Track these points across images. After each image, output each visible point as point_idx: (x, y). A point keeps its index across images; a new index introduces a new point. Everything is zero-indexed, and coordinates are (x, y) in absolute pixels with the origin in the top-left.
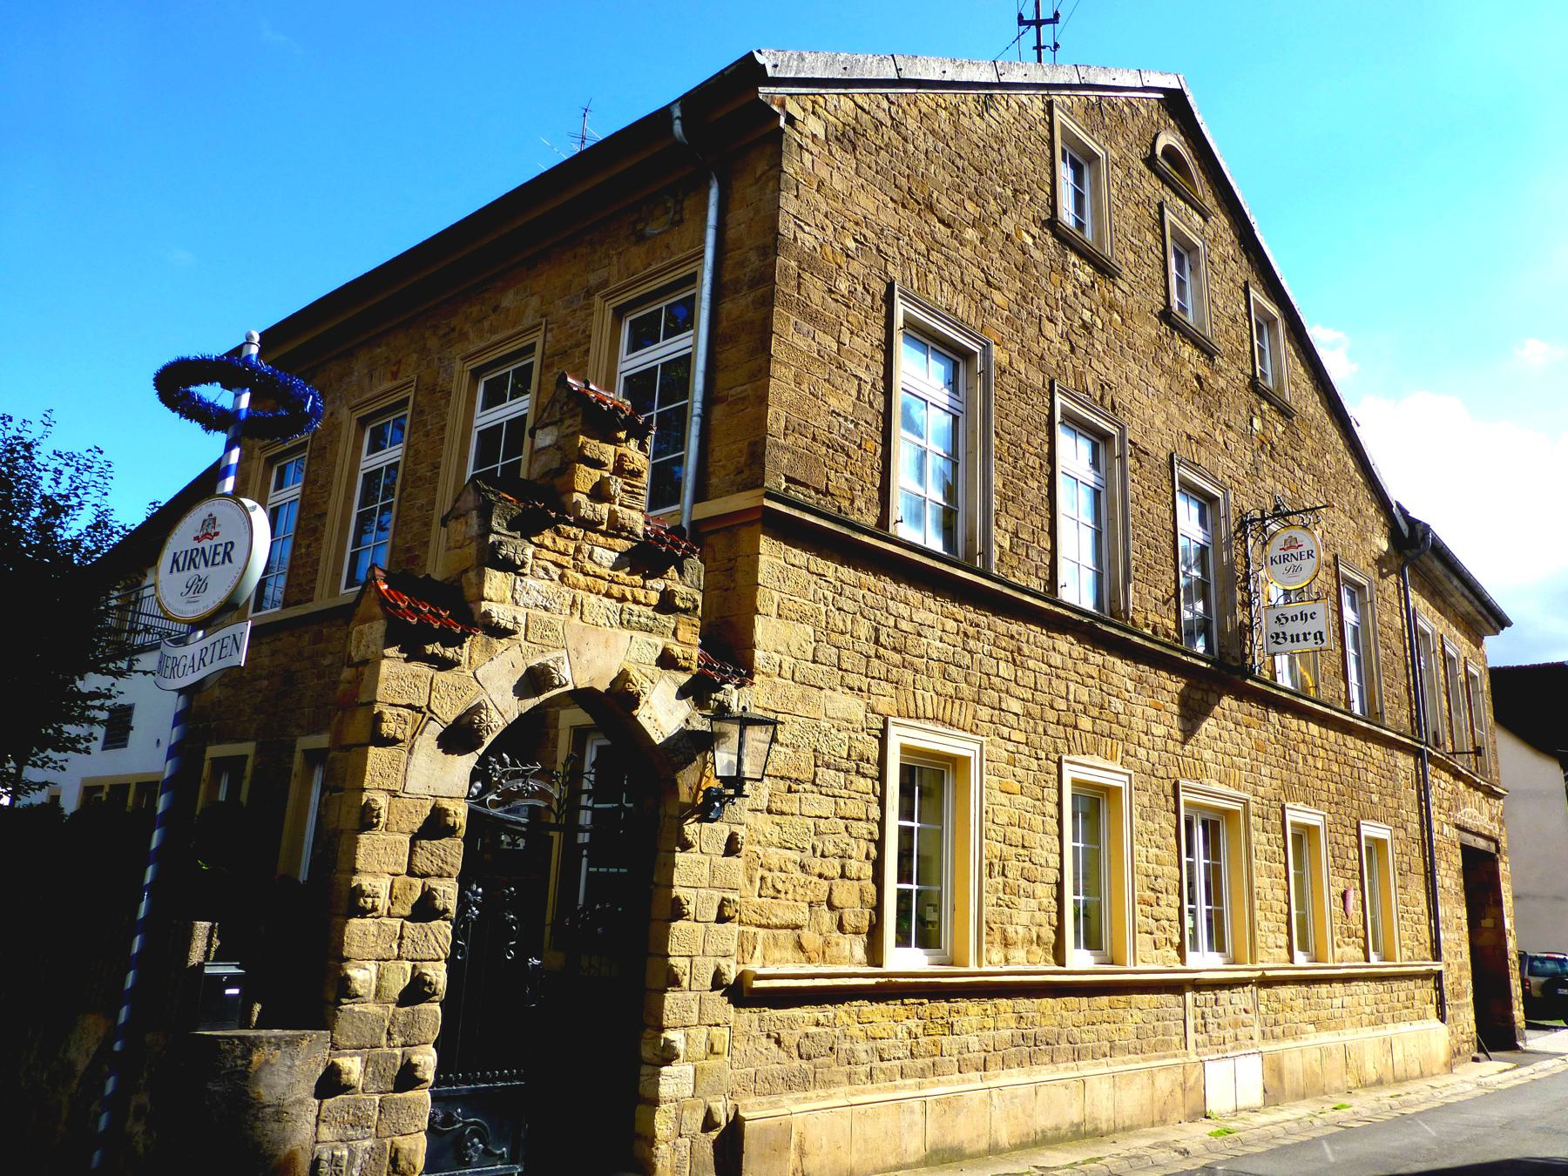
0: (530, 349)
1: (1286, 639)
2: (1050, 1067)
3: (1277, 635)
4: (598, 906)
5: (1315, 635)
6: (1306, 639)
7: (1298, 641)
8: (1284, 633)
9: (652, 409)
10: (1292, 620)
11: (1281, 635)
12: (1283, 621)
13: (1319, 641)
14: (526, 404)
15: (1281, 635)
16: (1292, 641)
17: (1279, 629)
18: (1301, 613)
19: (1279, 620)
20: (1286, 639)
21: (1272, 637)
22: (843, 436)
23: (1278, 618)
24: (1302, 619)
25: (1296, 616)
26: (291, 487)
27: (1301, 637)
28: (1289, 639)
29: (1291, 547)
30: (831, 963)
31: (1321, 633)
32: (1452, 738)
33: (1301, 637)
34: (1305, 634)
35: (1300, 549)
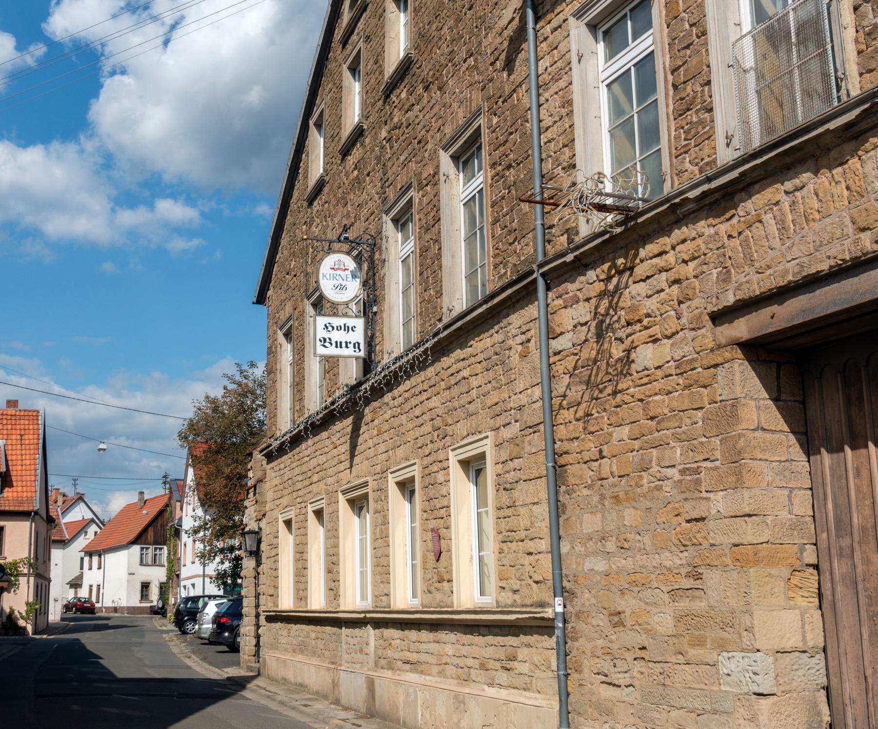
1: (331, 344)
2: (387, 491)
4: (227, 634)
5: (354, 344)
6: (347, 347)
7: (341, 347)
8: (330, 339)
10: (337, 329)
11: (328, 340)
12: (330, 328)
13: (357, 350)
15: (328, 340)
16: (337, 347)
18: (345, 325)
19: (327, 328)
20: (331, 344)
24: (345, 330)
25: (341, 327)
27: (344, 345)
28: (334, 344)
30: (501, 551)
31: (359, 344)
32: (832, 41)
33: (344, 345)
34: (346, 343)
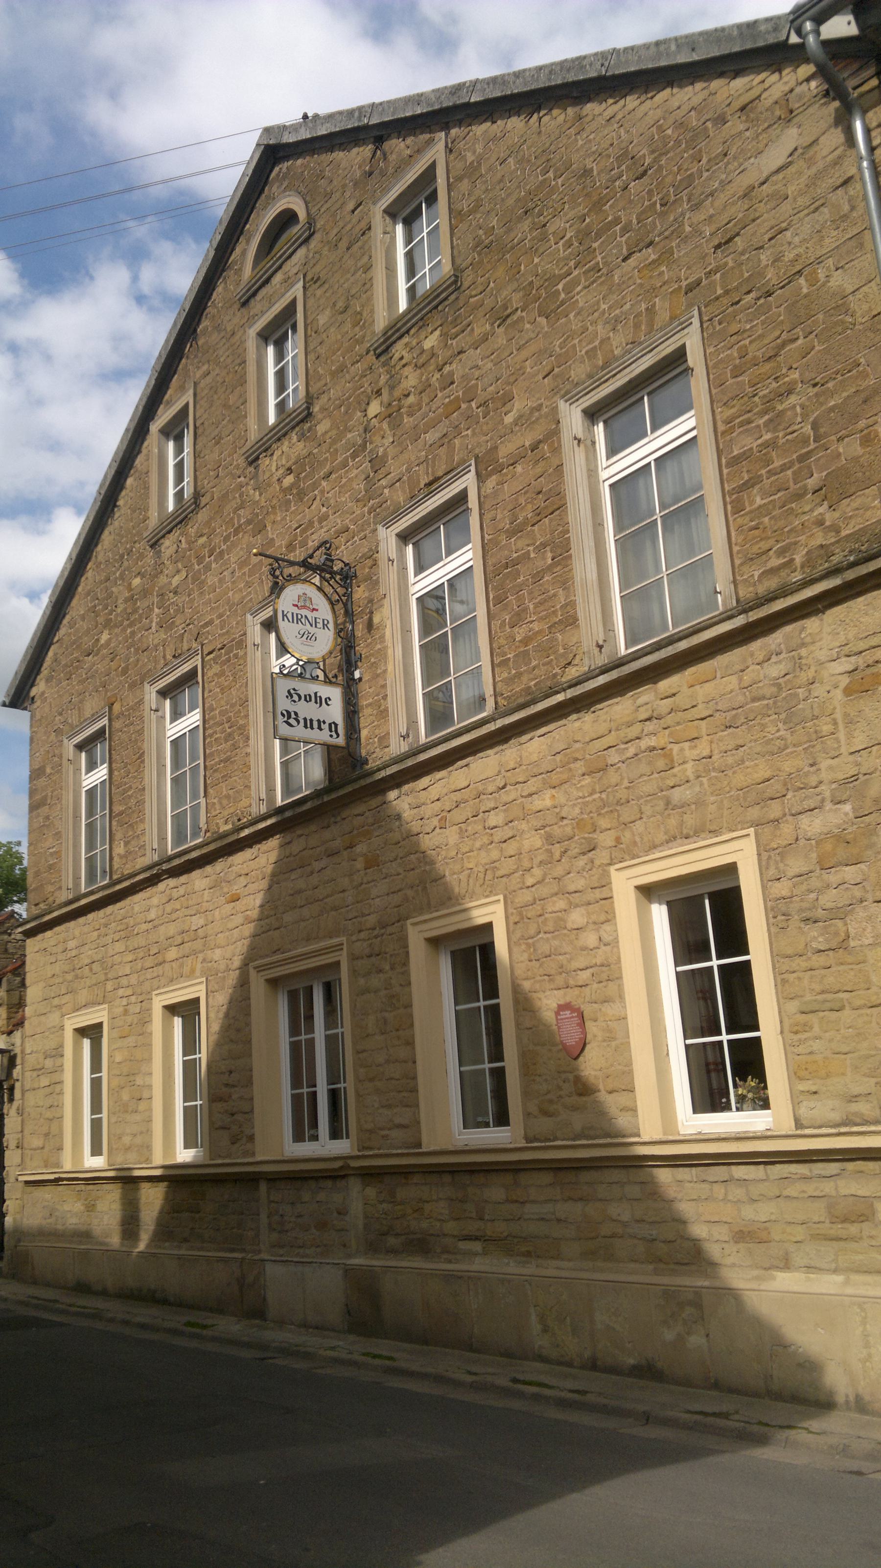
0: (339, 947)
1: (298, 722)
3: (288, 713)
5: (330, 725)
7: (312, 728)
9: (449, 675)
11: (293, 715)
12: (296, 698)
13: (335, 736)
14: (470, 555)
15: (293, 715)
17: (292, 708)
18: (316, 694)
20: (298, 722)
21: (283, 715)
22: (743, 761)
23: (289, 692)
26: (652, 437)
27: (315, 724)
29: (304, 607)
33: (315, 724)
35: (315, 614)
